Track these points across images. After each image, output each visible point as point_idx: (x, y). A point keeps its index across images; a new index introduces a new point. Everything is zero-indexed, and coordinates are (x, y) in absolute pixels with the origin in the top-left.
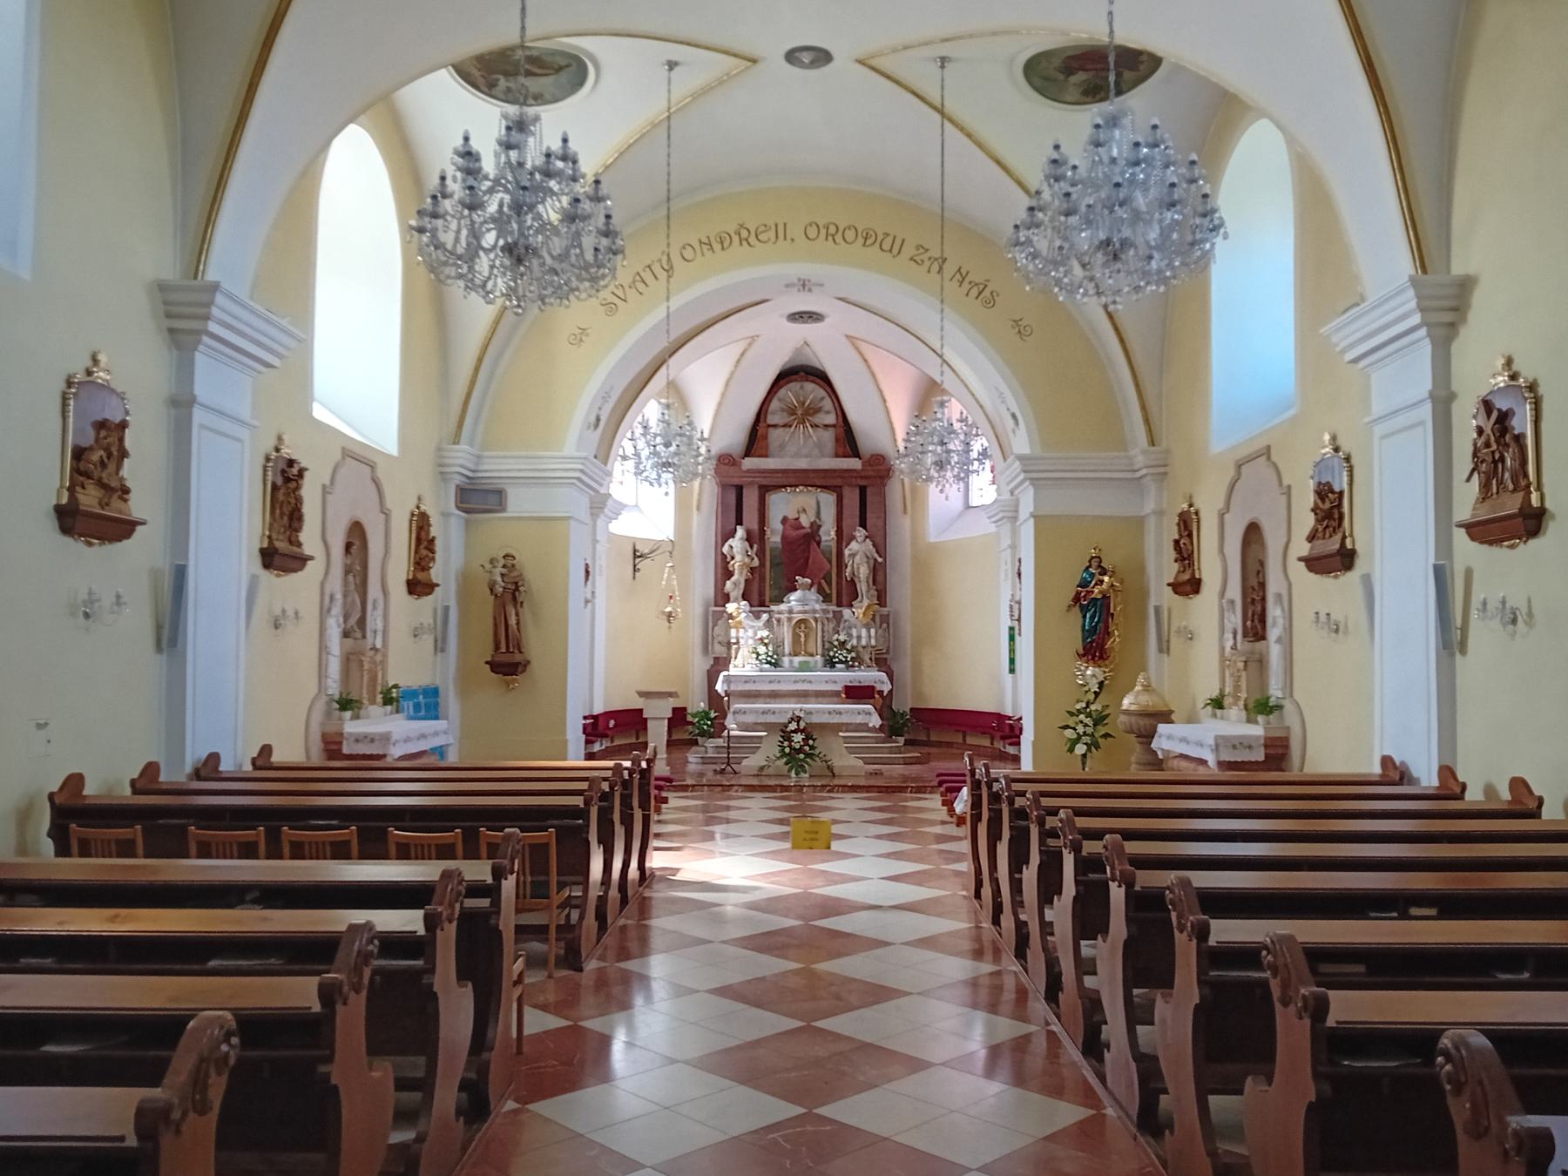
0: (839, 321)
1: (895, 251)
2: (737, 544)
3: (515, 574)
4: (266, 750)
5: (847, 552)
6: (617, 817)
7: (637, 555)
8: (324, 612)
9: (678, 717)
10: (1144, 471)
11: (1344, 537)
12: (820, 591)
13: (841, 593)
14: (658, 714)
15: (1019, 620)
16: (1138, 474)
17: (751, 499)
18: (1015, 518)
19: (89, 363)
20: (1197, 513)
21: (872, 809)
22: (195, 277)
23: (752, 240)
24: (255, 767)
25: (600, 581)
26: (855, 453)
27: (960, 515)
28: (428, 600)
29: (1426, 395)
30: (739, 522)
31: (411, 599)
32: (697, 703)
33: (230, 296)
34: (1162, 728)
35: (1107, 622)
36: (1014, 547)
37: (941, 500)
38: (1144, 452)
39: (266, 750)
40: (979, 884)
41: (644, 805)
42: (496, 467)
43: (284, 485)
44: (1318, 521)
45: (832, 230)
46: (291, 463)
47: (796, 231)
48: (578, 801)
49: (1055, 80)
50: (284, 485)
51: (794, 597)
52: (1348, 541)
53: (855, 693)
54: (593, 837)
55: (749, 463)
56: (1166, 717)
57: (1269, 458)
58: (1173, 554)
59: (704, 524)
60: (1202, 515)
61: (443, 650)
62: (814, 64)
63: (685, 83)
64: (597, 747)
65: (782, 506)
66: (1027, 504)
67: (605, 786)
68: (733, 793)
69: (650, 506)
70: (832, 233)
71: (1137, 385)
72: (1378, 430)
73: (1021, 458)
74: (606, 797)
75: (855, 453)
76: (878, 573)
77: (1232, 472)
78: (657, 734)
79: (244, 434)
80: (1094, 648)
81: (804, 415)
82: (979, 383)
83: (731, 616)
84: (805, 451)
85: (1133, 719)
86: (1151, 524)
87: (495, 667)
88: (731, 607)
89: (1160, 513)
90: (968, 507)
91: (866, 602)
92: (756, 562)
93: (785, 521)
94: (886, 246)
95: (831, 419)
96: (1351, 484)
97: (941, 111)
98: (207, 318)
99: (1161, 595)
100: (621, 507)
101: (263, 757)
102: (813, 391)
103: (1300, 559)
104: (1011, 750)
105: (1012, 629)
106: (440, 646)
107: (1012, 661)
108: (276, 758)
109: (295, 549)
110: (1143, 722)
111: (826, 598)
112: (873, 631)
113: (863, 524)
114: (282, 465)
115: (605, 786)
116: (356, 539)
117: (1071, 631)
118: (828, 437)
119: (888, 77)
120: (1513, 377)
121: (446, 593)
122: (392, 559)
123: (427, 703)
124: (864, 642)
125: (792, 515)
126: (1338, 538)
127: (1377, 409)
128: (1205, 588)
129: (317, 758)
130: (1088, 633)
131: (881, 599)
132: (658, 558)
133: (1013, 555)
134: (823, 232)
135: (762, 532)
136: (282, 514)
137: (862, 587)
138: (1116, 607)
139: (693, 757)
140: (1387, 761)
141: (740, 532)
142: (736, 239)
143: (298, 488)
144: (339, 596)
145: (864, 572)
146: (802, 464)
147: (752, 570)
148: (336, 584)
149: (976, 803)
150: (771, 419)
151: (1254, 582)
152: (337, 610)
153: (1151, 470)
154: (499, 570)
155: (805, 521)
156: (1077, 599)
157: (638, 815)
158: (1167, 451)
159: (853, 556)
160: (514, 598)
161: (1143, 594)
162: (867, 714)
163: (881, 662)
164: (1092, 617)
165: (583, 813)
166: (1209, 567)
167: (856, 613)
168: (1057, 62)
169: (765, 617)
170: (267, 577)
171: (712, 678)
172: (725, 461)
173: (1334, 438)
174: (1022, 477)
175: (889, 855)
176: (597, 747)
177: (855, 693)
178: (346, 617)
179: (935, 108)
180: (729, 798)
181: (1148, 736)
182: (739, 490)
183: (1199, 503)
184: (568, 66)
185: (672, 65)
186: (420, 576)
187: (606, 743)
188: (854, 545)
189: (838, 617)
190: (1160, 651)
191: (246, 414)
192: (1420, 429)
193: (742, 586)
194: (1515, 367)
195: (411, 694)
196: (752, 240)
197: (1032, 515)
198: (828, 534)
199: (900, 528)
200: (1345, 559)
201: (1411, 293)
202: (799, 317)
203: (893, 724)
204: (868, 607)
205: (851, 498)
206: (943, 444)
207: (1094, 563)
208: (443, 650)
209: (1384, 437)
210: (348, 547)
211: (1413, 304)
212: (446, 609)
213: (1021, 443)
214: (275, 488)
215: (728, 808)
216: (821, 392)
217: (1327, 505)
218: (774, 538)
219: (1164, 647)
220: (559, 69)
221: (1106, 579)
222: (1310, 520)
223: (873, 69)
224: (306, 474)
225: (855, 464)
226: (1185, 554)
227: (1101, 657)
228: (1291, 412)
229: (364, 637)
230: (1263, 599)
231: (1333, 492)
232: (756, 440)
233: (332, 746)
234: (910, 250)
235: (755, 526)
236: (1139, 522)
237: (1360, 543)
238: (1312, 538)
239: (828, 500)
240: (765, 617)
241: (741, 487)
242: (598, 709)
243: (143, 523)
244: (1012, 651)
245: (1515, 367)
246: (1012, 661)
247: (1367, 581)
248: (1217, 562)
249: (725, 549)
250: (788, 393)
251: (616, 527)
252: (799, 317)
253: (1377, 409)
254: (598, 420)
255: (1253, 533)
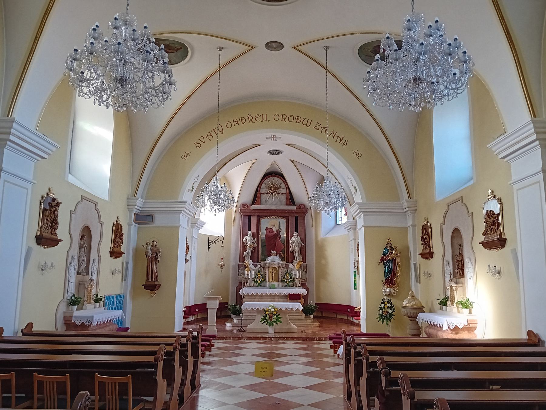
0: (288, 153)
1: (308, 125)
2: (248, 238)
3: (156, 249)
4: (30, 325)
5: (290, 241)
6: (177, 363)
7: (209, 242)
8: (68, 265)
9: (223, 307)
10: (407, 209)
11: (501, 233)
12: (280, 256)
13: (289, 257)
14: (213, 306)
15: (358, 268)
16: (405, 210)
17: (254, 220)
18: (355, 228)
19: (48, 191)
20: (430, 225)
21: (300, 349)
22: (8, 116)
23: (254, 120)
24: (23, 335)
25: (193, 253)
26: (294, 204)
27: (333, 228)
28: (119, 260)
29: (541, 169)
30: (249, 230)
31: (112, 259)
32: (232, 302)
33: (18, 124)
34: (421, 315)
35: (394, 269)
36: (355, 240)
37: (326, 220)
38: (407, 201)
39: (30, 325)
40: (349, 395)
41: (195, 354)
42: (152, 206)
43: (50, 210)
44: (488, 227)
45: (284, 117)
46: (54, 200)
47: (270, 117)
48: (151, 359)
49: (371, 56)
50: (50, 210)
51: (270, 258)
52: (503, 235)
53: (293, 297)
54: (159, 376)
55: (253, 207)
56: (421, 309)
57: (462, 202)
58: (421, 242)
59: (235, 230)
60: (432, 226)
61: (125, 280)
62: (276, 49)
63: (226, 56)
64: (190, 319)
65: (266, 223)
66: (361, 222)
67: (195, 334)
68: (242, 341)
69: (214, 222)
70: (284, 118)
71: (403, 176)
72: (516, 187)
73: (358, 203)
74: (184, 345)
75: (294, 204)
76: (303, 250)
77: (446, 208)
78: (212, 315)
79: (29, 186)
80: (390, 280)
81: (275, 189)
82: (341, 171)
83: (245, 266)
84: (274, 203)
85: (408, 310)
86: (410, 230)
87: (147, 287)
88: (246, 262)
89: (414, 226)
90: (336, 224)
91: (298, 261)
92: (256, 245)
93: (267, 229)
94: (305, 123)
95: (284, 191)
96: (502, 210)
97: (326, 69)
98: (9, 134)
99: (416, 258)
100: (203, 224)
101: (28, 330)
102: (277, 180)
103: (480, 243)
104: (356, 321)
105: (355, 272)
106: (124, 278)
107: (355, 285)
108: (35, 329)
109: (53, 236)
110: (412, 312)
111: (283, 259)
112: (300, 272)
113: (297, 231)
114: (49, 200)
115: (195, 334)
116: (86, 234)
117: (380, 272)
118: (283, 198)
119: (305, 54)
120: (428, 222)
121: (128, 256)
122: (104, 242)
123: (118, 302)
124: (249, 277)
125: (270, 227)
126: (498, 233)
127: (514, 178)
128: (435, 256)
129: (61, 329)
130: (386, 274)
131: (304, 260)
132: (219, 244)
133: (355, 243)
134: (281, 117)
135: (258, 233)
136: (48, 222)
137: (296, 255)
138: (398, 263)
139: (228, 325)
140: (530, 333)
141: (250, 233)
142: (247, 120)
143: (56, 210)
144: (76, 257)
145: (297, 249)
146: (273, 208)
147: (254, 248)
148: (75, 252)
149: (348, 354)
150: (262, 191)
151: (458, 253)
152: (75, 263)
153: (410, 209)
154: (149, 247)
155: (274, 229)
156: (382, 260)
157: (191, 360)
158: (416, 201)
159: (293, 243)
160: (156, 259)
161: (409, 259)
162: (298, 306)
163: (304, 285)
164: (389, 267)
165: (154, 366)
166: (437, 247)
167: (295, 266)
168: (371, 49)
169: (259, 266)
170: (38, 249)
171: (238, 289)
172: (243, 205)
173: (492, 192)
174: (359, 211)
175: (306, 374)
176: (190, 319)
177: (293, 297)
178: (79, 267)
179: (324, 67)
180: (242, 343)
181: (414, 318)
182: (250, 217)
183: (430, 221)
184: (181, 48)
185: (221, 49)
186: (116, 249)
187: (195, 317)
188: (293, 239)
189: (287, 266)
190: (417, 281)
191: (30, 178)
192: (538, 184)
193: (250, 254)
194: (494, 194)
195: (109, 298)
196: (254, 120)
197: (363, 226)
198: (283, 234)
199: (311, 232)
200: (502, 243)
201: (532, 126)
202: (271, 152)
203: (307, 311)
204: (299, 263)
205: (292, 220)
206: (328, 195)
207: (389, 246)
208: (125, 280)
209: (518, 190)
210: (83, 237)
211: (533, 130)
212: (127, 263)
213: (358, 198)
214: (45, 210)
215: (241, 348)
216: (281, 181)
217: (492, 220)
218: (263, 236)
219: (418, 280)
220: (177, 50)
221: (394, 252)
222: (483, 227)
223: (299, 51)
224: (61, 205)
225: (293, 208)
226: (426, 240)
227: (392, 284)
228: (472, 182)
229: (88, 274)
230: (463, 260)
231: (494, 214)
232: (256, 199)
233: (69, 323)
234: (313, 124)
235: (255, 231)
236: (407, 228)
237: (508, 234)
238: (484, 234)
239: (283, 222)
240: (259, 266)
241: (250, 214)
242: (191, 304)
243: (62, 241)
244: (355, 280)
245: (494, 194)
246: (355, 285)
247: (514, 252)
248: (440, 244)
249: (244, 239)
250: (268, 182)
251: (201, 231)
252: (271, 152)
253: (514, 178)
254: (193, 188)
255: (456, 233)
